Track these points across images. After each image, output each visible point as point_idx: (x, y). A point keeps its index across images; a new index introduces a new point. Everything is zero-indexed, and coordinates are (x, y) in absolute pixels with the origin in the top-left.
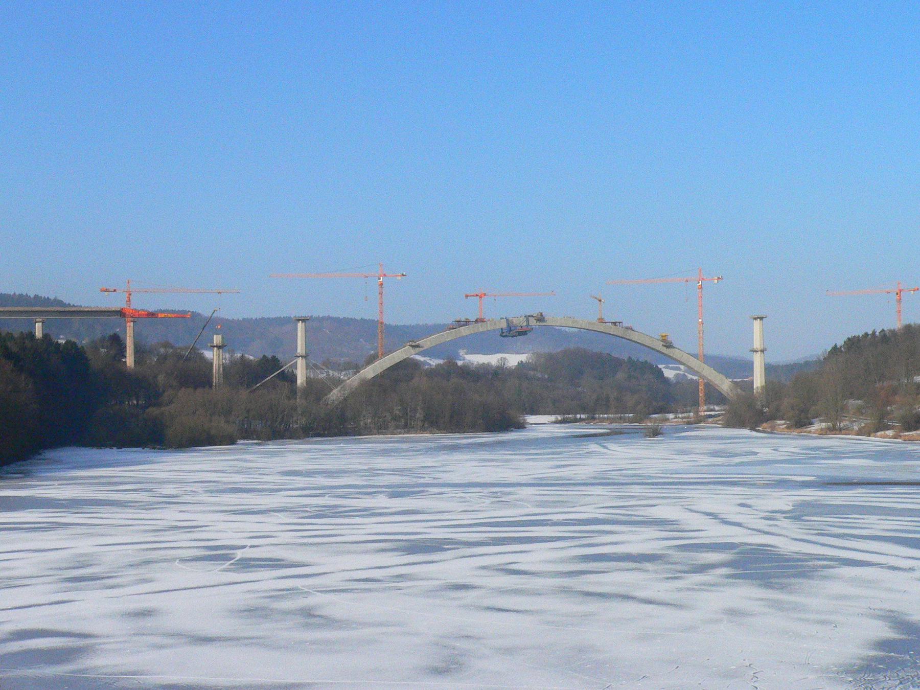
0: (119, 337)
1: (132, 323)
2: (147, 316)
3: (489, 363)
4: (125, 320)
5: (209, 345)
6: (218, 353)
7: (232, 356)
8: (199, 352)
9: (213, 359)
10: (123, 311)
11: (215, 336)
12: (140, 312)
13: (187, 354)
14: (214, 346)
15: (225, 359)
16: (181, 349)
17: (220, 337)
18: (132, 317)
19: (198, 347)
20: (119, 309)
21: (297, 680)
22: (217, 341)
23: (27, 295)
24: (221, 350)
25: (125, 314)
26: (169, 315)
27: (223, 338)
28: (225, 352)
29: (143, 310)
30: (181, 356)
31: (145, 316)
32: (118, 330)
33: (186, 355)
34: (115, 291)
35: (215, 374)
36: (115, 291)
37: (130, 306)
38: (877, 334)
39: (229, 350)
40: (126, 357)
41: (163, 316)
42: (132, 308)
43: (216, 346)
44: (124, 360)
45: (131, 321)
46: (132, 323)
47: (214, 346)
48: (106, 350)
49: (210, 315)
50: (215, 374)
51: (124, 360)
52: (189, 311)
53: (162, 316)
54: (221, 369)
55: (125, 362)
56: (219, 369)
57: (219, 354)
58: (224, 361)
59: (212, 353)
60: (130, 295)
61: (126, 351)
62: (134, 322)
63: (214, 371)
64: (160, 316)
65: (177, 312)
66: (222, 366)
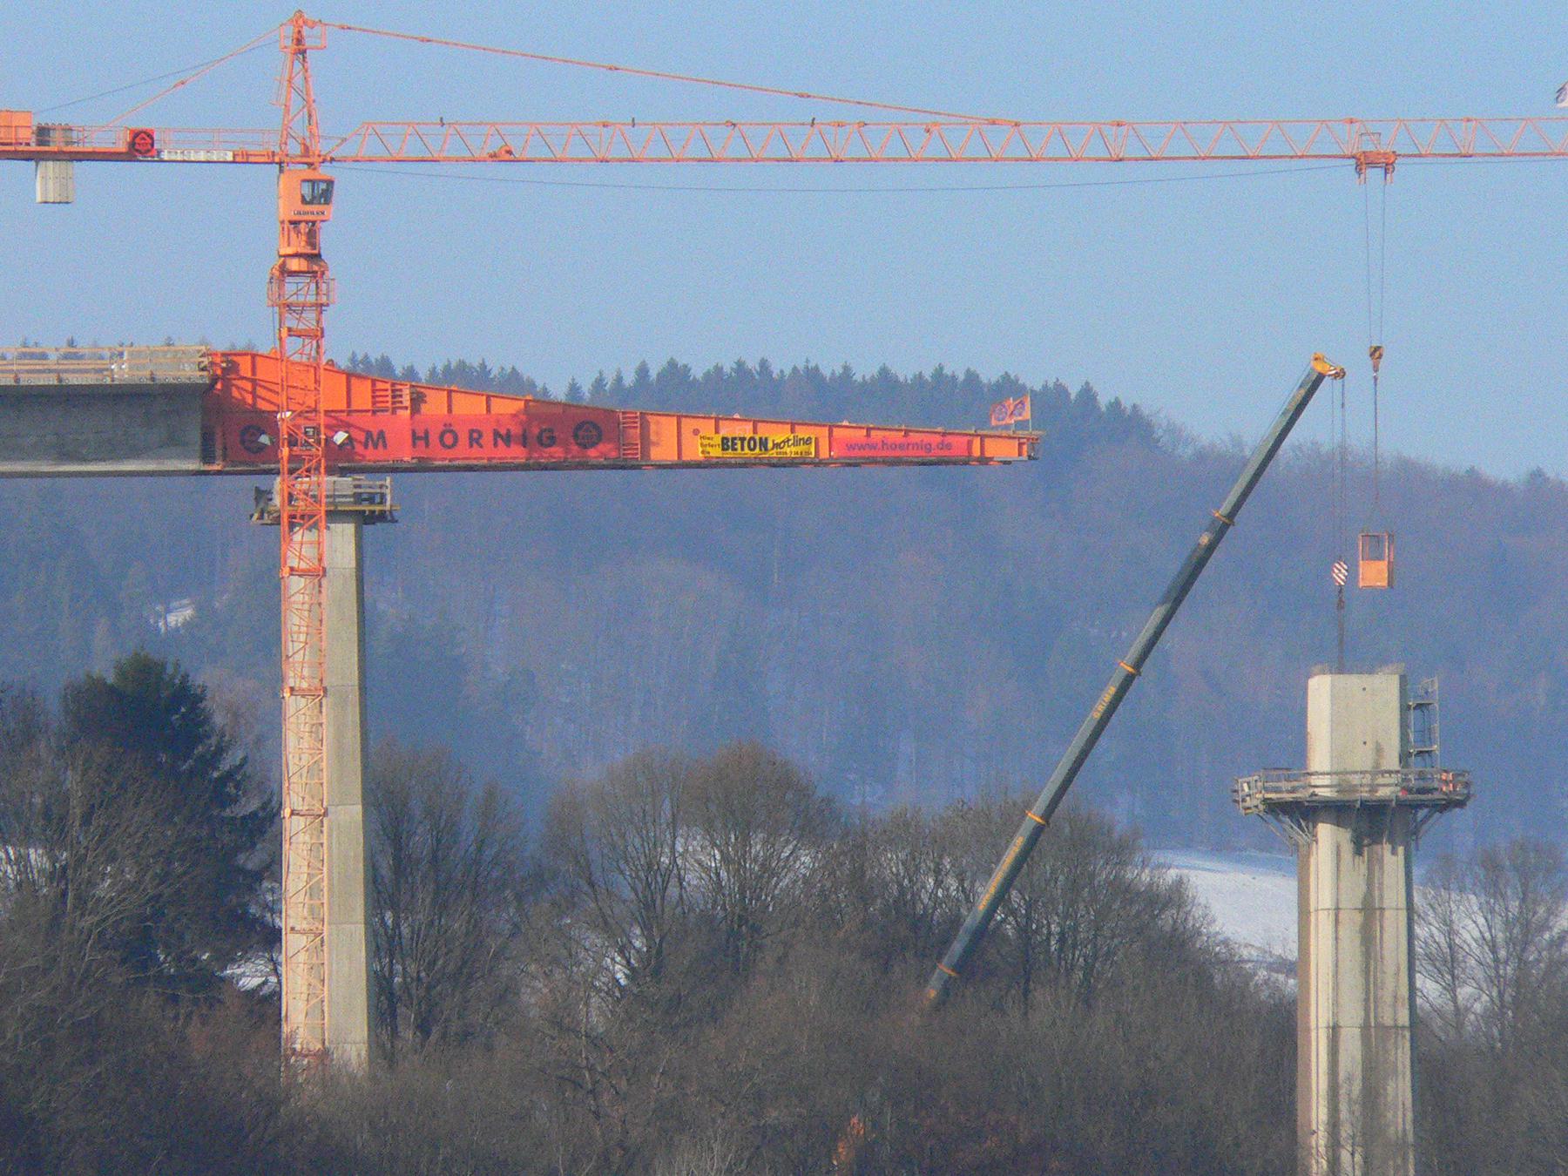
0: (187, 699)
1: (349, 529)
2: (517, 453)
3: (1472, 471)
4: (262, 495)
5: (1252, 790)
6: (1353, 896)
7: (1524, 931)
8: (1140, 875)
9: (1297, 968)
10: (241, 391)
11: (1321, 689)
12: (435, 405)
13: (986, 894)
14: (1306, 812)
15: (1449, 963)
16: (903, 830)
17: (1382, 691)
18: (340, 462)
19: (1120, 813)
20: (189, 373)
21: (882, 166)
22: (1337, 753)
23: (939, 373)
24: (1392, 862)
25: (267, 422)
26: (776, 435)
27: (1413, 708)
28: (1447, 876)
29: (461, 378)
30: (919, 923)
31: (488, 452)
32: (180, 616)
33: (970, 921)
34: (141, 146)
35: (1320, 1140)
36: (141, 146)
37: (317, 335)
38: (653, 374)
39: (1492, 865)
40: (272, 938)
41: (703, 442)
42: (339, 349)
43: (1337, 811)
44: (249, 975)
45: (335, 515)
46: (349, 529)
47: (1306, 812)
48: (36, 856)
49: (1256, 430)
50: (1320, 1140)
51: (249, 975)
52: (1008, 387)
53: (695, 452)
54: (1400, 1090)
55: (267, 1006)
56: (1371, 1097)
57: (1370, 910)
58: (1429, 987)
59: (1290, 886)
60: (323, 193)
61: (273, 868)
62: (367, 516)
63: (1317, 1113)
64: (663, 452)
65: (867, 388)
66: (1402, 1055)
